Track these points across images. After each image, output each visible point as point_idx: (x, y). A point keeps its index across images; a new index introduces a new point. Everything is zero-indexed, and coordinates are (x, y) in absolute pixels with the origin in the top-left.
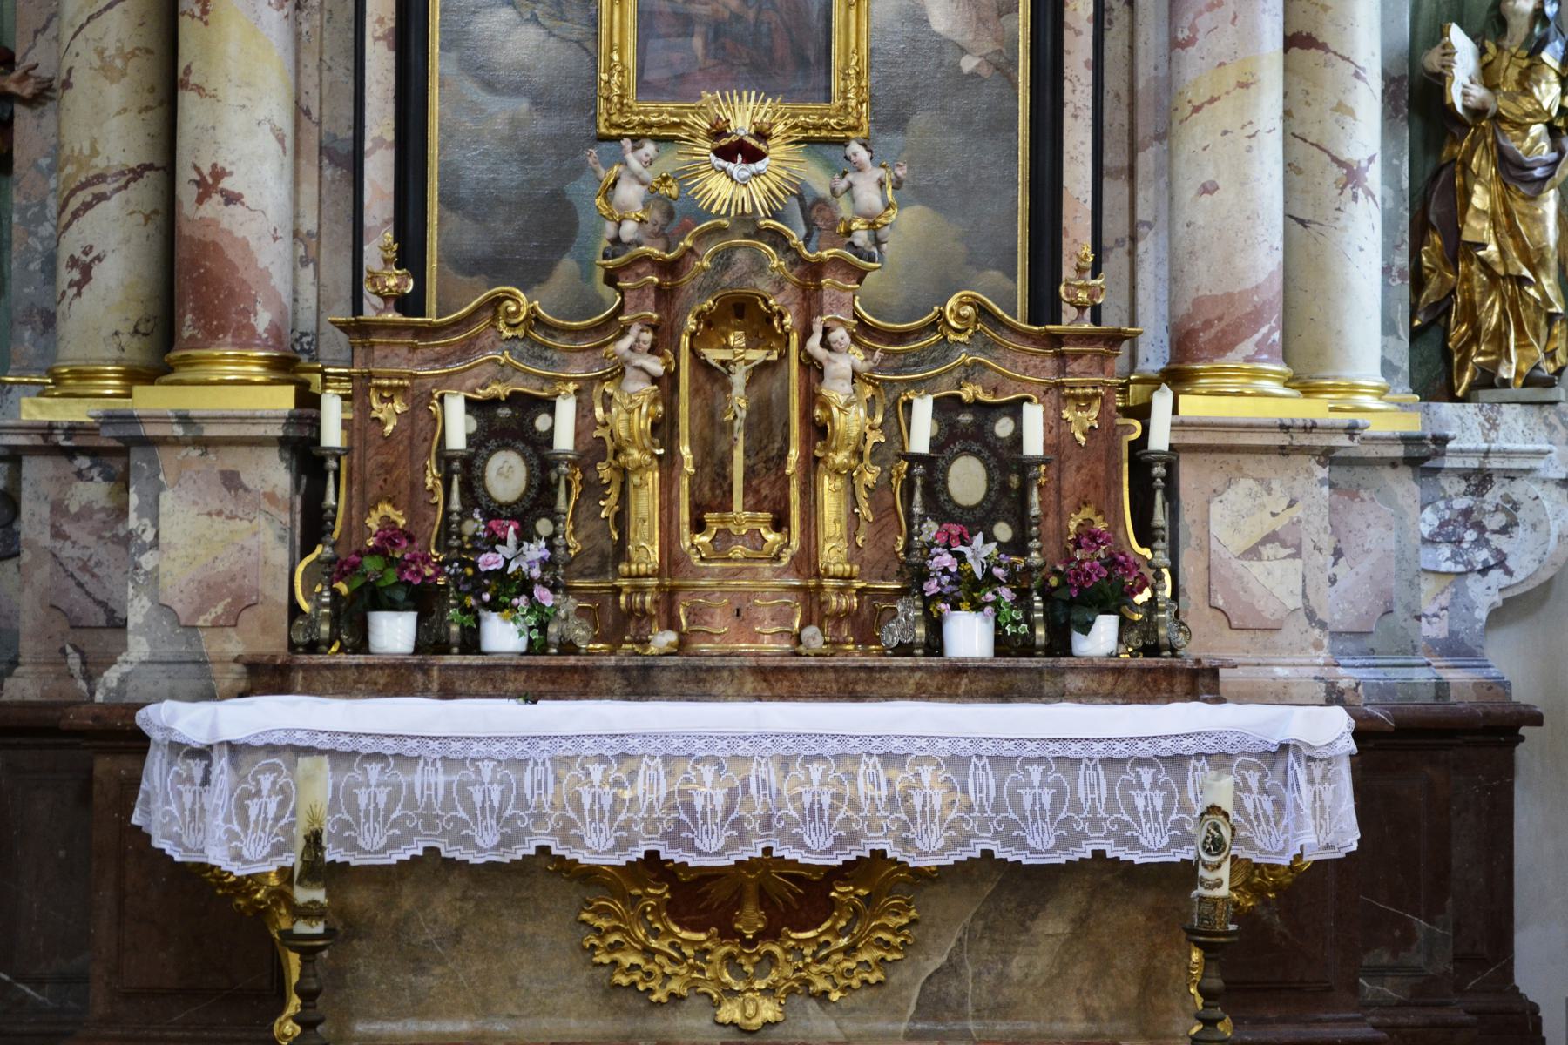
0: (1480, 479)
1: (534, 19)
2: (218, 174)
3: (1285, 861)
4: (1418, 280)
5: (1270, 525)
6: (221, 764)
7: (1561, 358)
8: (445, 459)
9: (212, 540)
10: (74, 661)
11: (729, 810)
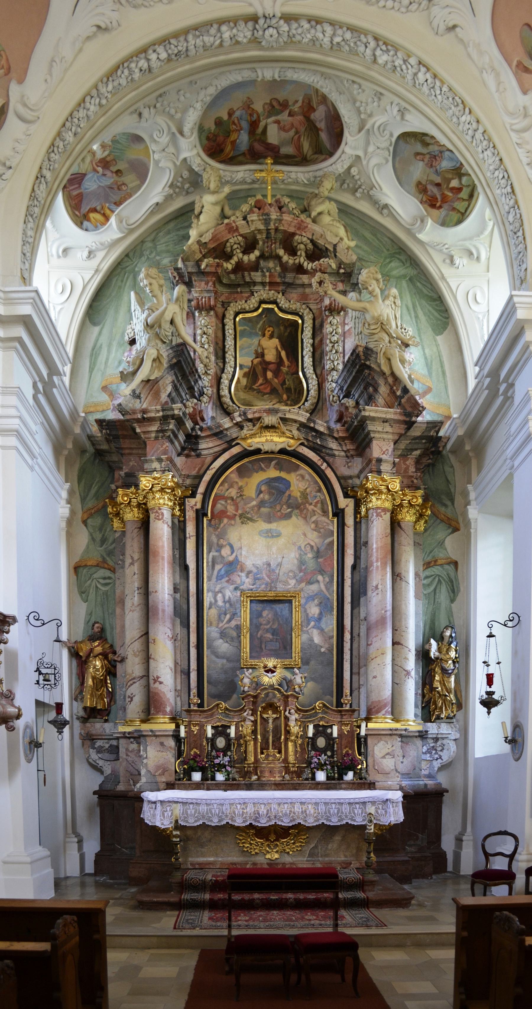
0: (436, 740)
1: (227, 642)
2: (158, 677)
3: (387, 824)
4: (423, 696)
5: (387, 751)
6: (159, 805)
7: (455, 712)
8: (207, 739)
9: (157, 757)
10: (131, 782)
11: (267, 814)
